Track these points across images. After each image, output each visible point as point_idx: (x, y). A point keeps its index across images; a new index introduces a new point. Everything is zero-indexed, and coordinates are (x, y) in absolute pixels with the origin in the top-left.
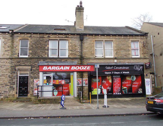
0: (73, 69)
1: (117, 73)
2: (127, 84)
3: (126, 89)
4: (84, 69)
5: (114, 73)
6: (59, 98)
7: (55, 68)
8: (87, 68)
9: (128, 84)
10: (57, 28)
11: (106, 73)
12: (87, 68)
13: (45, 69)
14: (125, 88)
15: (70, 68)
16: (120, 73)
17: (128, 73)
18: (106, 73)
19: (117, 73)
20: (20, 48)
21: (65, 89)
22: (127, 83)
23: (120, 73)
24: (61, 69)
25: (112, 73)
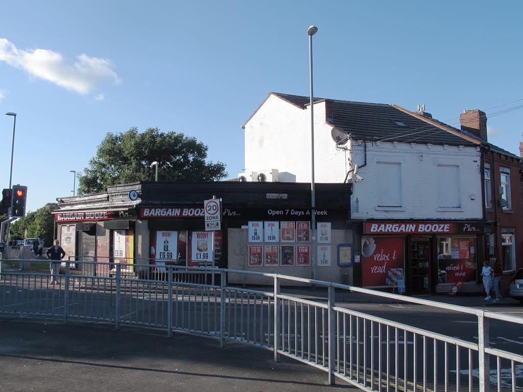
0: (422, 231)
1: (296, 213)
2: (457, 271)
3: (444, 274)
4: (440, 230)
5: (289, 212)
6: (224, 318)
7: (391, 229)
8: (443, 229)
9: (459, 271)
10: (64, 353)
11: (270, 212)
12: (443, 229)
13: (389, 226)
14: (442, 272)
15: (417, 228)
16: (305, 213)
17: (325, 213)
18: (270, 212)
19: (296, 213)
20: (148, 280)
21: (253, 302)
22: (458, 268)
23: (305, 213)
24: (381, 231)
25: (285, 212)
